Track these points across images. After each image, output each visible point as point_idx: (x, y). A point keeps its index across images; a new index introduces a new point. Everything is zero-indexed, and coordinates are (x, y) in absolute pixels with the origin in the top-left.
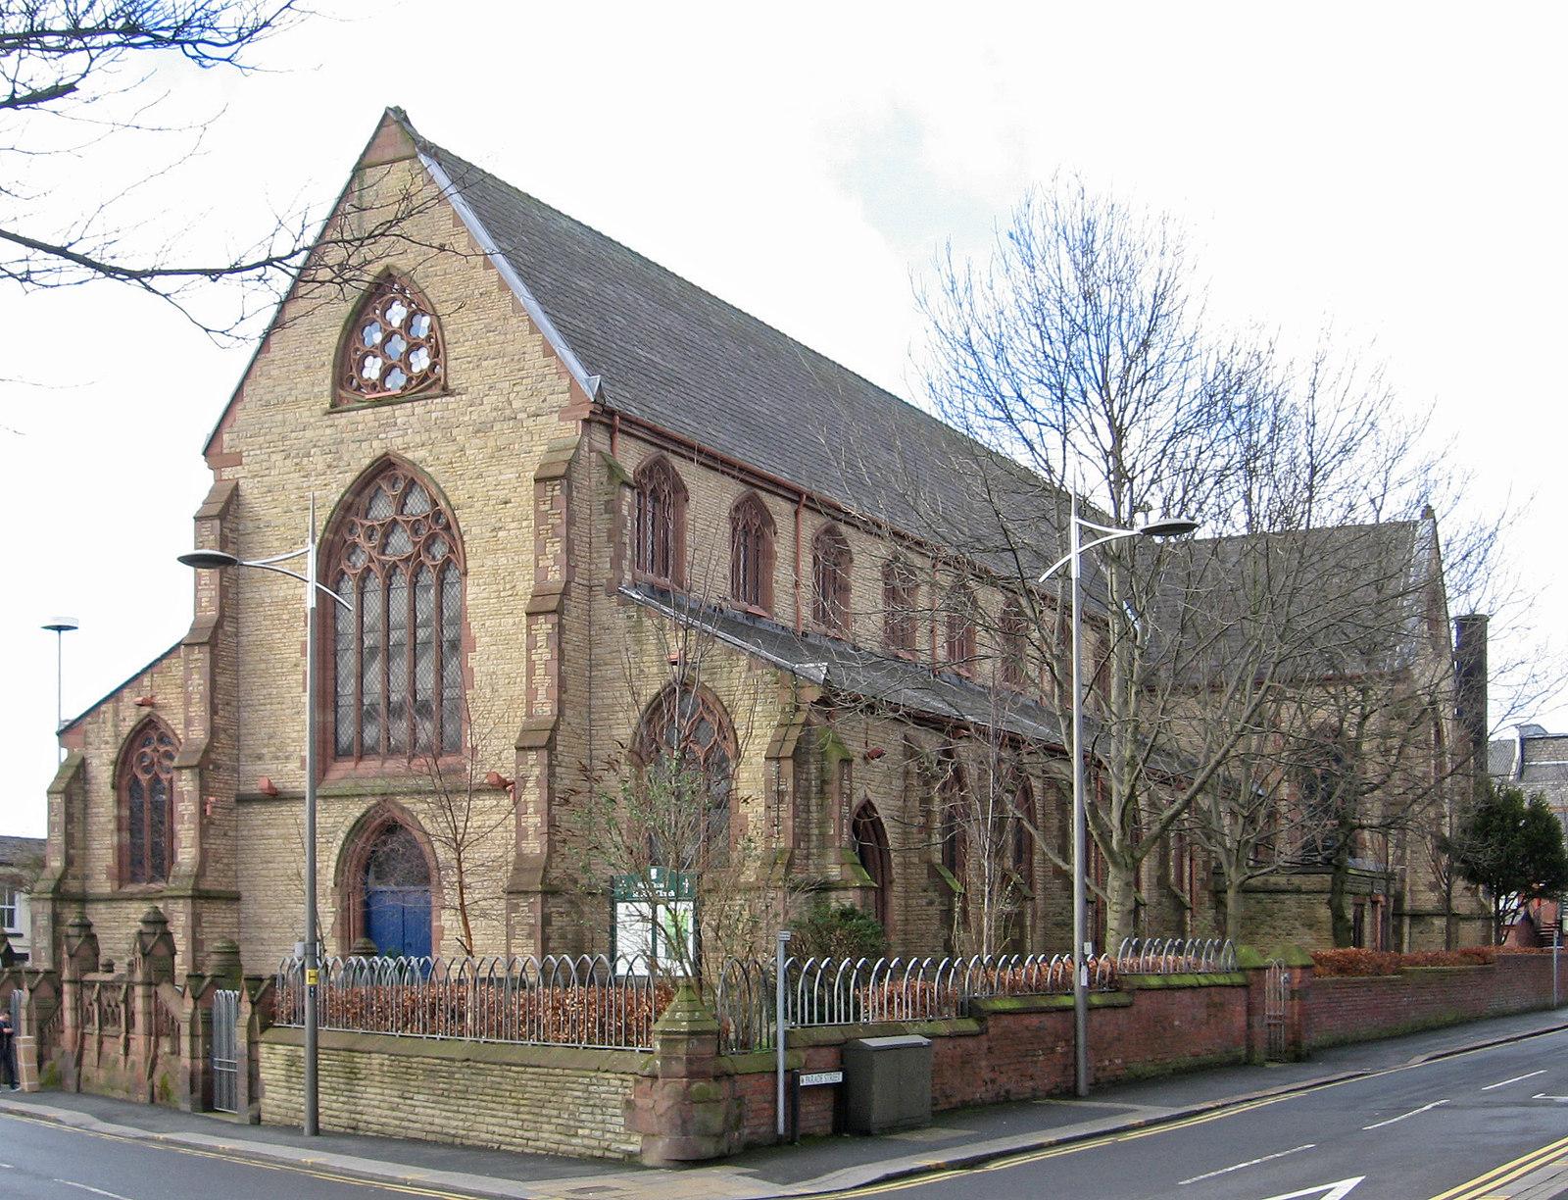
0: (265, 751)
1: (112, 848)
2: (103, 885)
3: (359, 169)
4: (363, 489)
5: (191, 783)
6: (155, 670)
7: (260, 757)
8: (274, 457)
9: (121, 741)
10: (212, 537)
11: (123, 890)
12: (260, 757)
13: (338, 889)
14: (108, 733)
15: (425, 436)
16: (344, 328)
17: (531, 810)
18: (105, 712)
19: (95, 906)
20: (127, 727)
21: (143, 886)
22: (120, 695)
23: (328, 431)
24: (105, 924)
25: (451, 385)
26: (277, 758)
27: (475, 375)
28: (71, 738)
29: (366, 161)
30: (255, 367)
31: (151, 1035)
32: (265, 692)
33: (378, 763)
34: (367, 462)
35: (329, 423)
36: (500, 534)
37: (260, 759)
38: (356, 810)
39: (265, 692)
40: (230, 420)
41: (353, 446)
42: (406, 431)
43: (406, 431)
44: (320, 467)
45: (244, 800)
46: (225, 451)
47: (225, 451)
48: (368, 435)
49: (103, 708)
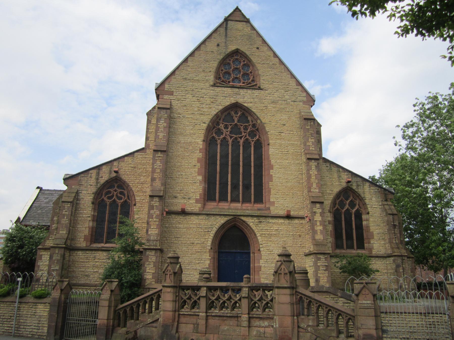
0: (178, 195)
1: (89, 227)
2: (82, 244)
3: (226, 20)
4: (224, 112)
5: (158, 203)
6: (120, 160)
7: (176, 197)
8: (188, 95)
9: (99, 185)
10: (166, 115)
11: (92, 246)
12: (176, 197)
13: (212, 251)
14: (93, 181)
15: (252, 100)
16: (220, 62)
17: (318, 224)
18: (91, 173)
19: (76, 252)
20: (102, 181)
21: (102, 245)
22: (101, 168)
23: (212, 91)
24: (81, 260)
25: (262, 87)
26: (184, 198)
27: (271, 86)
28: (71, 181)
29: (229, 18)
30: (181, 66)
31: (294, 316)
32: (180, 173)
33: (215, 204)
34: (228, 104)
35: (213, 89)
36: (282, 134)
37: (176, 198)
38: (222, 221)
39: (180, 173)
40: (169, 80)
41: (222, 98)
42: (246, 98)
43: (246, 98)
44: (208, 102)
45: (170, 213)
46: (165, 90)
47: (165, 90)
48: (226, 97)
49: (91, 172)
